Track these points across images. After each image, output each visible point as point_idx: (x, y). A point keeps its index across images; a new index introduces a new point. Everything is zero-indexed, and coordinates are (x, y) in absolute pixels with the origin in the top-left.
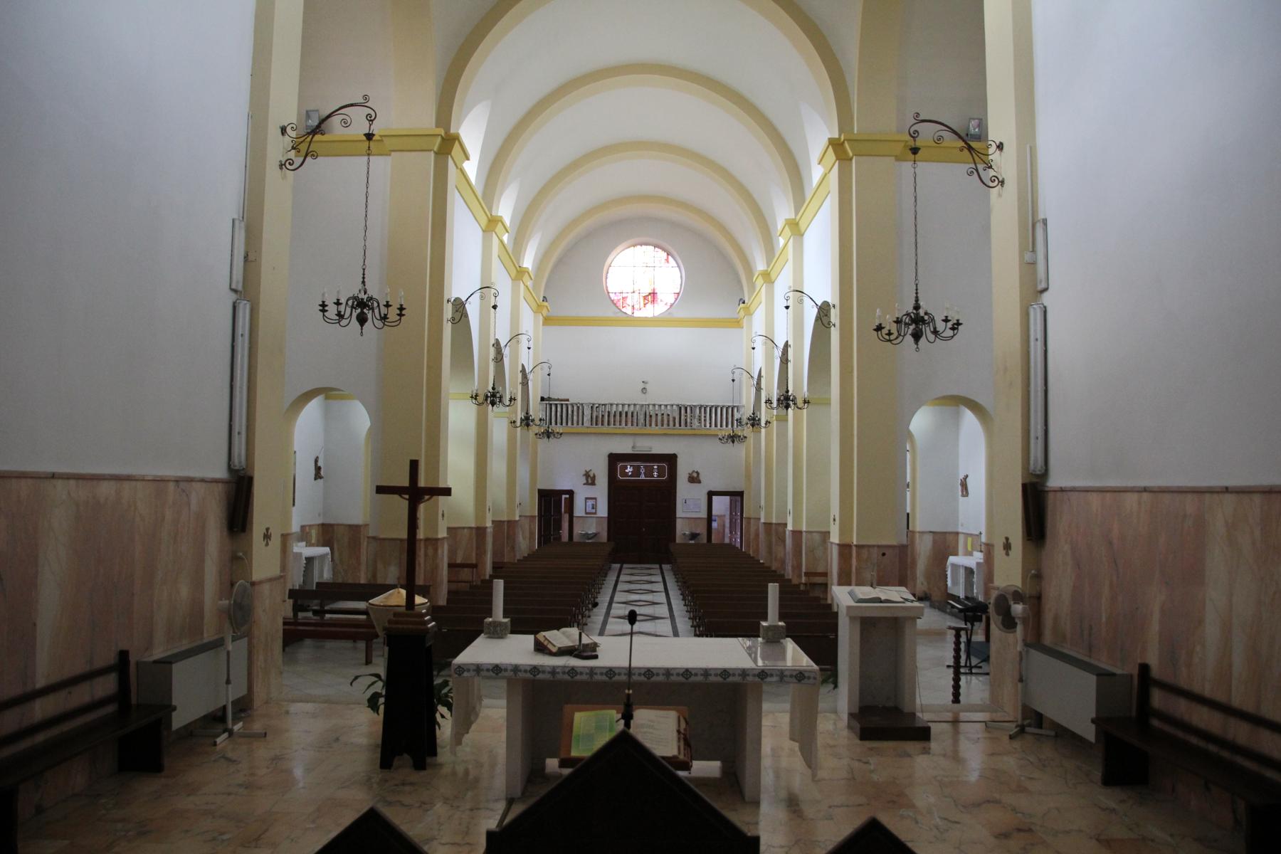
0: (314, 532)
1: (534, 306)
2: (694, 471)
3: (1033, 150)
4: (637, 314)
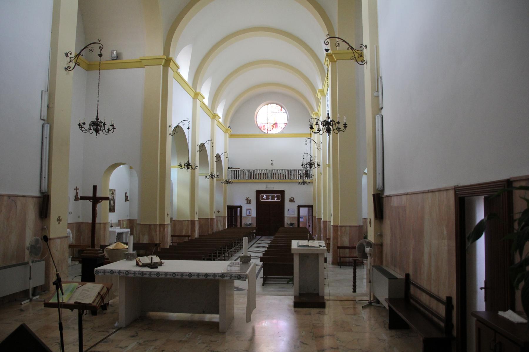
0: (125, 223)
1: (224, 130)
2: (292, 197)
3: (377, 47)
4: (269, 132)
